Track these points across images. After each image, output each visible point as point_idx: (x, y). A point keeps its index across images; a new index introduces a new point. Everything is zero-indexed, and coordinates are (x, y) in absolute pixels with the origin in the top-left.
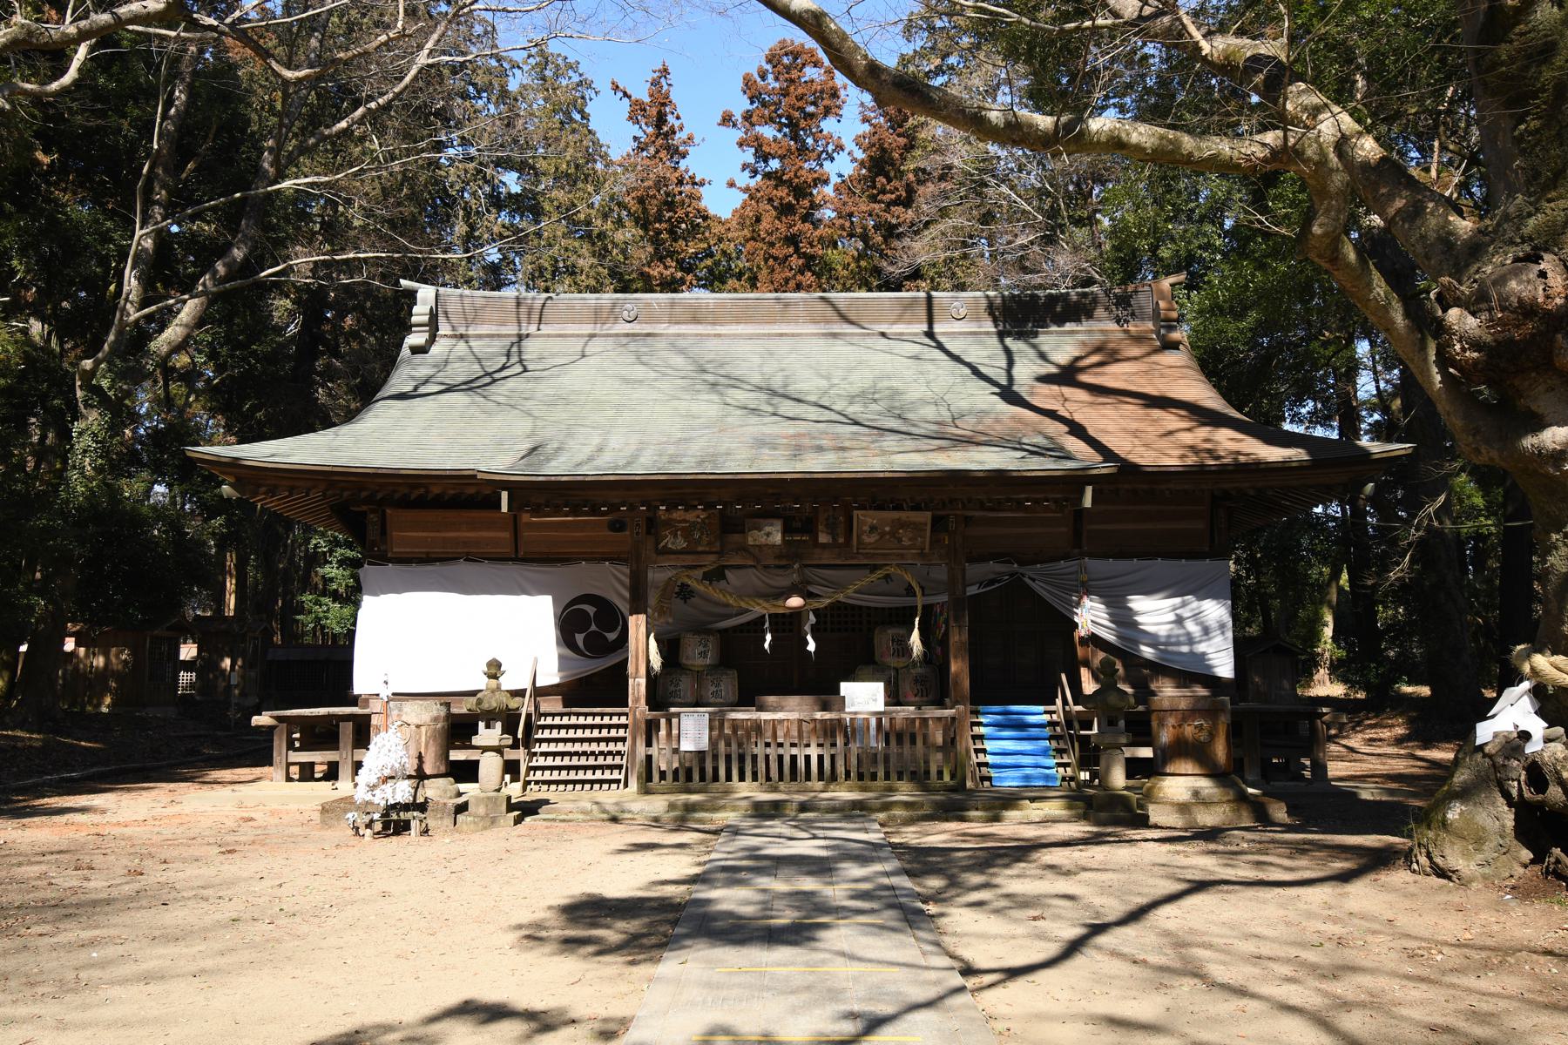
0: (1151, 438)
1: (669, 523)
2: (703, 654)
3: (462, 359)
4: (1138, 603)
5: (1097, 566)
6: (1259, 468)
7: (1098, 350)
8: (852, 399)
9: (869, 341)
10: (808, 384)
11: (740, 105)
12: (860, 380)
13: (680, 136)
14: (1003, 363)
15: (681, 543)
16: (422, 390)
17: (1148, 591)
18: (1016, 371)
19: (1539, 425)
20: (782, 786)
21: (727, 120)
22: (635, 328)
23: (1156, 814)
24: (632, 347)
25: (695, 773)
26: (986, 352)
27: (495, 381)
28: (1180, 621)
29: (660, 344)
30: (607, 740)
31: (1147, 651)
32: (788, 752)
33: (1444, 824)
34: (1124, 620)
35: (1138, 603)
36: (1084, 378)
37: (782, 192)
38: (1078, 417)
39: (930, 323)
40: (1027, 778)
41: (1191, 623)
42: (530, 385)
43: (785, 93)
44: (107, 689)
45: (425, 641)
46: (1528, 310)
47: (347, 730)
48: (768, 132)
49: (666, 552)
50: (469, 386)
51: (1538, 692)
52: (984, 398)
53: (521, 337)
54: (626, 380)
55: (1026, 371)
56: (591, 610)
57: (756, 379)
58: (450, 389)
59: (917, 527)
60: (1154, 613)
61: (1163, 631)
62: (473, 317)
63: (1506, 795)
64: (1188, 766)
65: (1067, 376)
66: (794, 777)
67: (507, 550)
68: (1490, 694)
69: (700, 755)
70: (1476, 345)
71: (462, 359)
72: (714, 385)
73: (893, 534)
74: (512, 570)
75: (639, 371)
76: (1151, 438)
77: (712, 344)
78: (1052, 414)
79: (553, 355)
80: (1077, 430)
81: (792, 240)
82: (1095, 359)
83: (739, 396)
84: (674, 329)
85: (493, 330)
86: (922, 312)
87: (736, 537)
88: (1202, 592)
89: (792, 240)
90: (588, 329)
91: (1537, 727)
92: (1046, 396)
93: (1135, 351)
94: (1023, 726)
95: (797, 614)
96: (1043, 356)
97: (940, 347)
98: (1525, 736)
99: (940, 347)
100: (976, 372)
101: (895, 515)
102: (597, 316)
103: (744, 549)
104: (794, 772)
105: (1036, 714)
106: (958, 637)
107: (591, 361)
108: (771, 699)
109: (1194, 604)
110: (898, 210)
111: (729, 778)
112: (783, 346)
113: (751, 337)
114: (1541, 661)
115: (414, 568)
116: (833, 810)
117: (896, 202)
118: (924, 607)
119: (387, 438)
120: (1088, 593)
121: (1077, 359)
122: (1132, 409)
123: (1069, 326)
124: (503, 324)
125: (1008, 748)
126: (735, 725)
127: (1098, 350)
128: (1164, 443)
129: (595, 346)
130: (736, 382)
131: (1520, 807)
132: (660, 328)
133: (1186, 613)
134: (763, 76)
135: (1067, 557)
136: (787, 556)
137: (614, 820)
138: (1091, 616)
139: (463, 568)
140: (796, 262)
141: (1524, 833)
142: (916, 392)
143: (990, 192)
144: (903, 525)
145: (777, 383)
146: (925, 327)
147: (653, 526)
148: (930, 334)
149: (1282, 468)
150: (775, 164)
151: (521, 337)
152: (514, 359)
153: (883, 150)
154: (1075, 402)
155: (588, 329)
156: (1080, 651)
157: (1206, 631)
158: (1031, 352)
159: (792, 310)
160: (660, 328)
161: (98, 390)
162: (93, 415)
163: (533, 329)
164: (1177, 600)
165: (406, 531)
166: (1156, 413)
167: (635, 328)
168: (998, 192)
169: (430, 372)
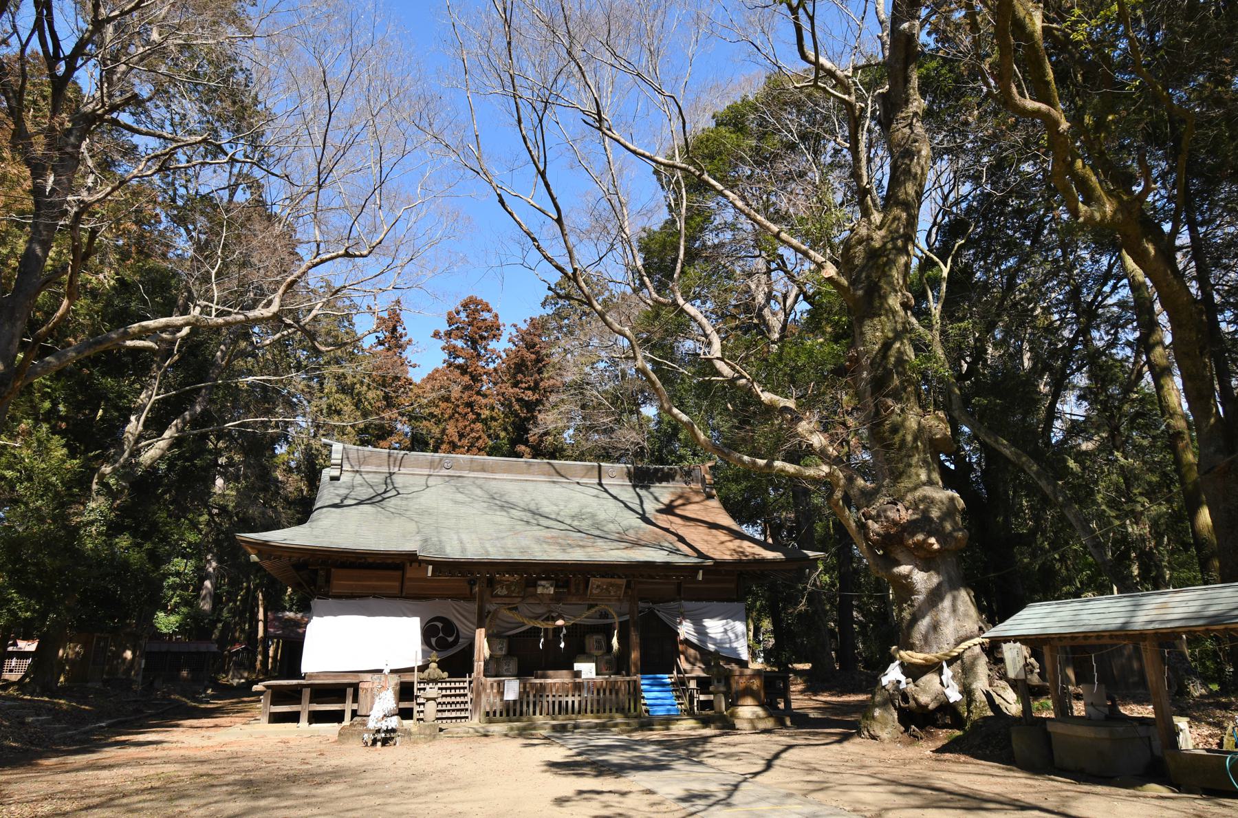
0: (715, 545)
1: (500, 582)
2: (501, 649)
3: (362, 485)
4: (708, 623)
5: (688, 605)
6: (763, 561)
7: (680, 497)
8: (573, 517)
9: (572, 486)
10: (547, 509)
11: (444, 327)
12: (574, 508)
13: (404, 339)
14: (638, 501)
15: (505, 592)
16: (346, 502)
17: (711, 617)
18: (645, 506)
19: (899, 564)
20: (560, 717)
21: (436, 335)
22: (451, 472)
23: (738, 724)
24: (452, 482)
25: (511, 712)
26: (628, 494)
27: (384, 499)
28: (726, 631)
29: (467, 482)
30: (455, 696)
31: (711, 647)
32: (564, 699)
33: (873, 718)
34: (701, 631)
35: (708, 623)
36: (678, 511)
37: (467, 378)
38: (680, 533)
39: (600, 479)
40: (669, 710)
41: (727, 631)
42: (404, 503)
43: (470, 324)
44: (62, 670)
45: (339, 642)
46: (895, 523)
47: (350, 691)
48: (460, 343)
49: (497, 596)
50: (370, 501)
51: (902, 665)
52: (635, 521)
53: (391, 474)
54: (456, 502)
55: (650, 507)
56: (440, 625)
57: (522, 504)
58: (361, 503)
59: (619, 587)
60: (715, 627)
61: (718, 636)
62: (363, 461)
63: (894, 705)
64: (749, 701)
65: (669, 510)
66: (573, 712)
67: (396, 592)
68: (301, 631)
69: (515, 701)
70: (878, 534)
71: (362, 485)
72: (502, 507)
73: (607, 589)
74: (399, 603)
75: (460, 497)
76: (715, 545)
77: (493, 483)
78: (667, 530)
79: (412, 485)
80: (682, 539)
81: (470, 405)
82: (680, 502)
83: (516, 513)
84: (472, 475)
85: (374, 469)
86: (596, 473)
87: (531, 589)
88: (735, 618)
89: (470, 405)
90: (426, 472)
91: (903, 678)
92: (663, 520)
93: (697, 499)
94: (664, 685)
95: (560, 628)
96: (656, 499)
97: (606, 491)
98: (899, 682)
99: (606, 491)
100: (626, 506)
101: (609, 580)
102: (432, 465)
103: (535, 595)
104: (563, 709)
105: (667, 679)
106: (635, 638)
107: (432, 489)
108: (551, 672)
109: (732, 623)
110: (530, 393)
111: (534, 713)
112: (530, 486)
113: (511, 480)
114: (902, 653)
115: (344, 601)
116: (590, 728)
117: (529, 388)
118: (621, 623)
119: (330, 529)
120: (684, 618)
121: (672, 501)
122: (702, 529)
123: (664, 484)
124: (380, 466)
125: (656, 697)
126: (533, 685)
127: (680, 497)
128: (722, 547)
129: (431, 481)
130: (513, 506)
131: (900, 711)
132: (465, 473)
133: (728, 627)
134: (458, 313)
135: (674, 600)
136: (557, 598)
137: (486, 736)
138: (686, 630)
139: (371, 602)
140: (471, 416)
141: (902, 720)
142: (602, 516)
143: (588, 393)
144: (612, 585)
145: (533, 507)
146: (597, 481)
147: (491, 583)
148: (600, 484)
149: (773, 562)
150: (460, 361)
151: (391, 474)
152: (390, 487)
153: (523, 360)
154: (676, 524)
155: (426, 472)
156: (681, 647)
157: (737, 637)
158: (651, 497)
159: (532, 468)
160: (465, 473)
161: (107, 485)
162: (101, 499)
163: (396, 470)
164: (724, 621)
165: (341, 581)
166: (714, 531)
167: (451, 472)
168: (591, 393)
169: (346, 492)
